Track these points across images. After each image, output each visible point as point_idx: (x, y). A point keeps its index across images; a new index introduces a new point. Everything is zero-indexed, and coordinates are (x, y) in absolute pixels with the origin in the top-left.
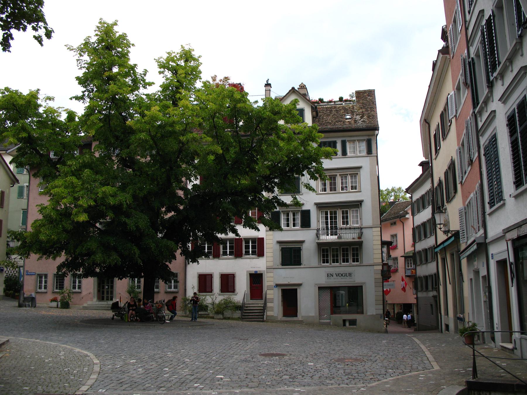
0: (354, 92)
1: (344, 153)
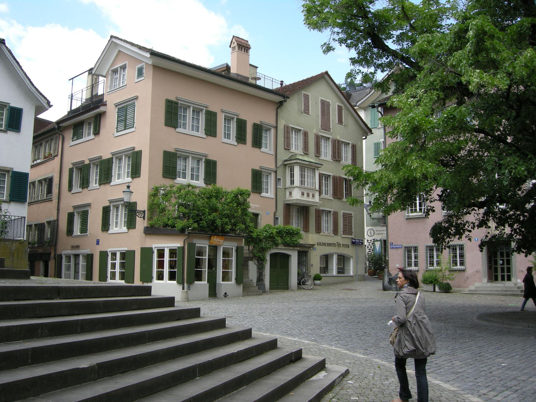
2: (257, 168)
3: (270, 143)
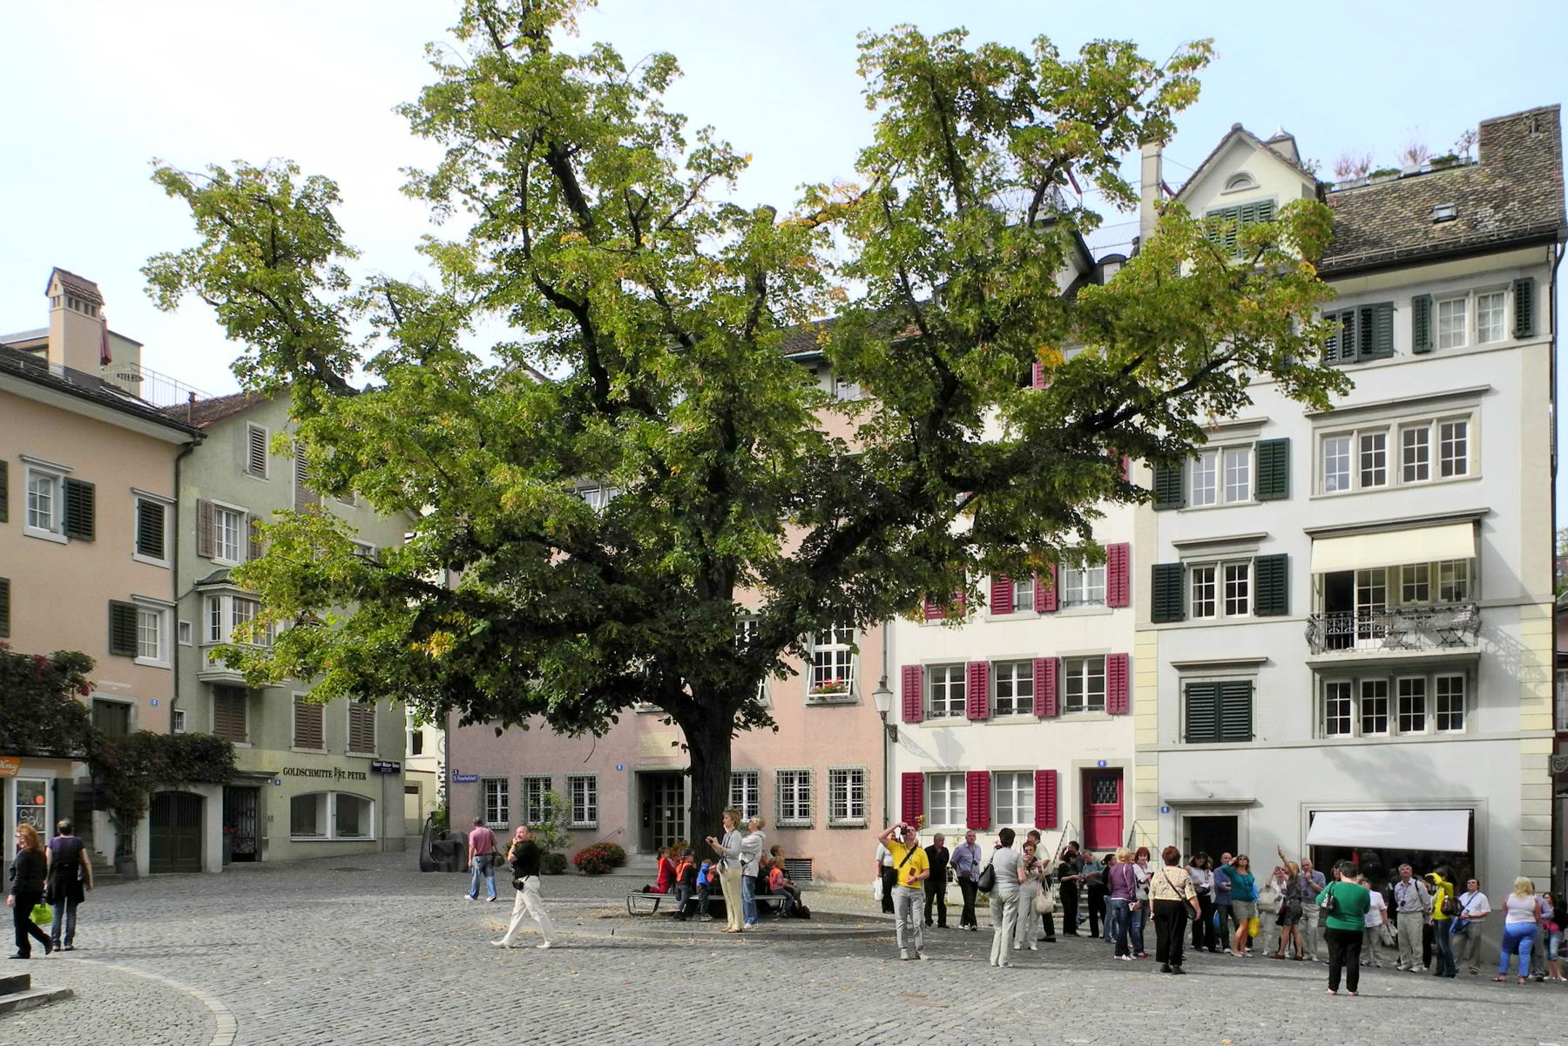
0: (1475, 128)
2: (124, 598)
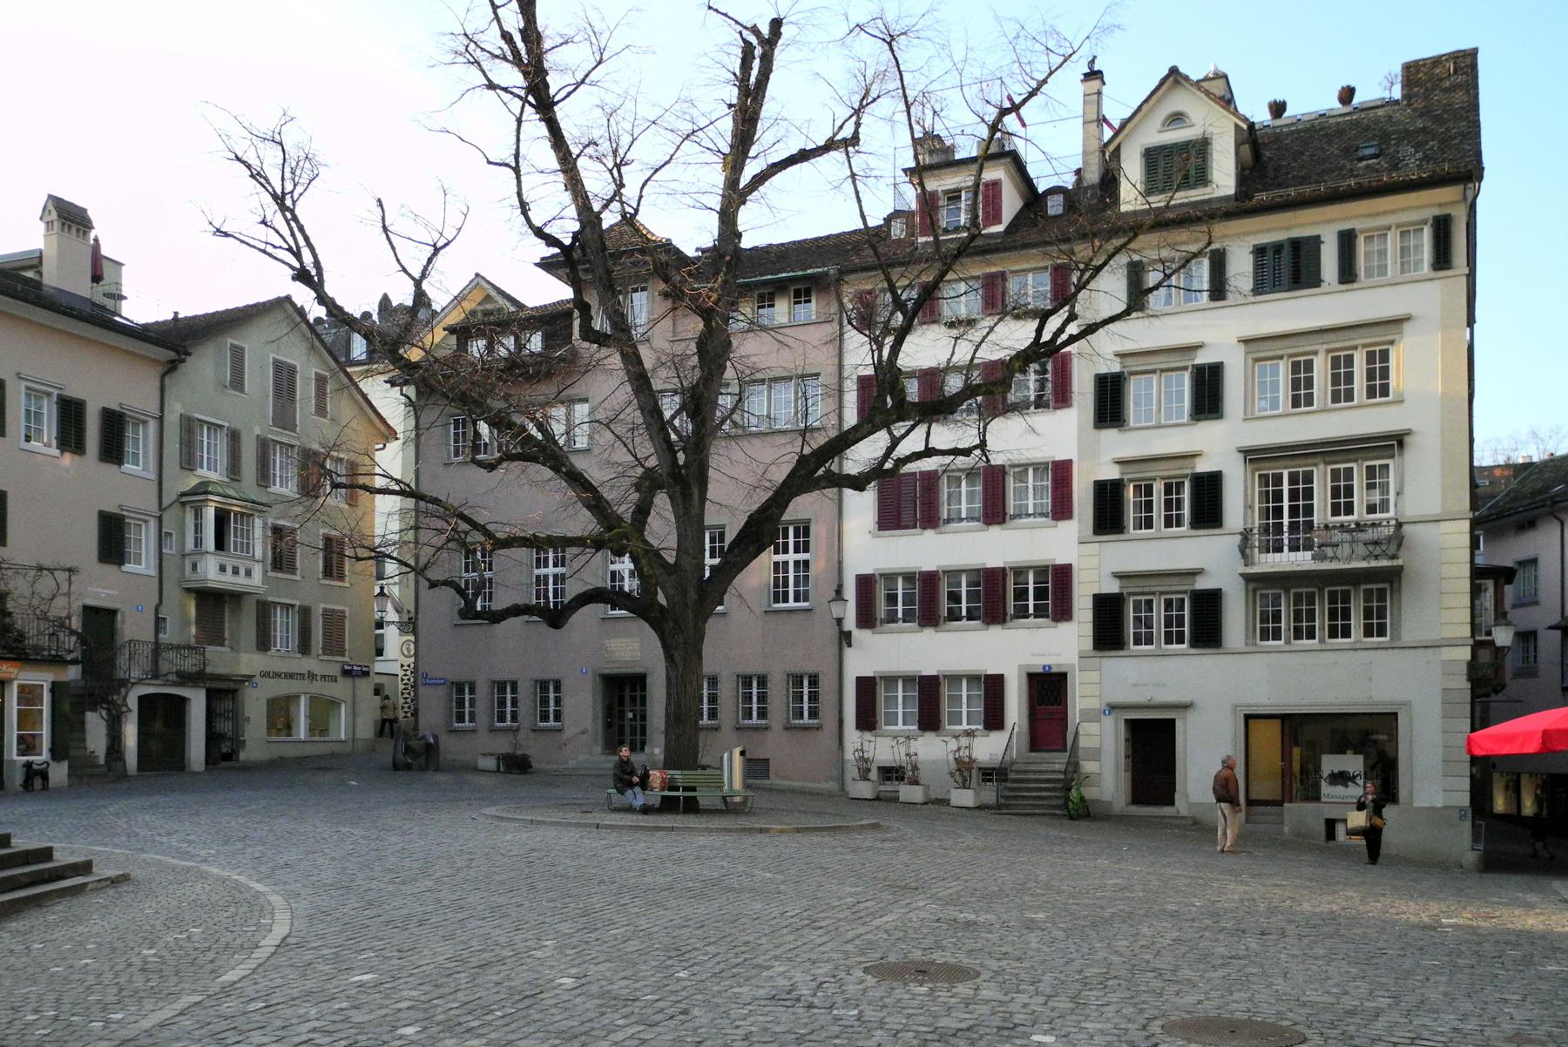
0: (1398, 70)
1: (1347, 274)
2: (111, 508)
3: (145, 453)
